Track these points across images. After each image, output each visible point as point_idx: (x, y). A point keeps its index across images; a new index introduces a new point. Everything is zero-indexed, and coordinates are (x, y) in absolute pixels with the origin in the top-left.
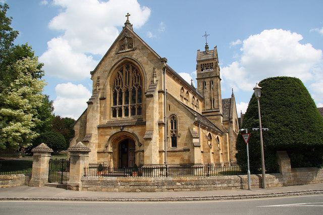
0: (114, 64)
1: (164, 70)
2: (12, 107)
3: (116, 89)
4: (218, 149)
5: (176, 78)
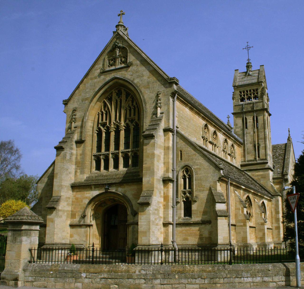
0: (97, 89)
1: (173, 97)
3: (102, 128)
4: (263, 221)
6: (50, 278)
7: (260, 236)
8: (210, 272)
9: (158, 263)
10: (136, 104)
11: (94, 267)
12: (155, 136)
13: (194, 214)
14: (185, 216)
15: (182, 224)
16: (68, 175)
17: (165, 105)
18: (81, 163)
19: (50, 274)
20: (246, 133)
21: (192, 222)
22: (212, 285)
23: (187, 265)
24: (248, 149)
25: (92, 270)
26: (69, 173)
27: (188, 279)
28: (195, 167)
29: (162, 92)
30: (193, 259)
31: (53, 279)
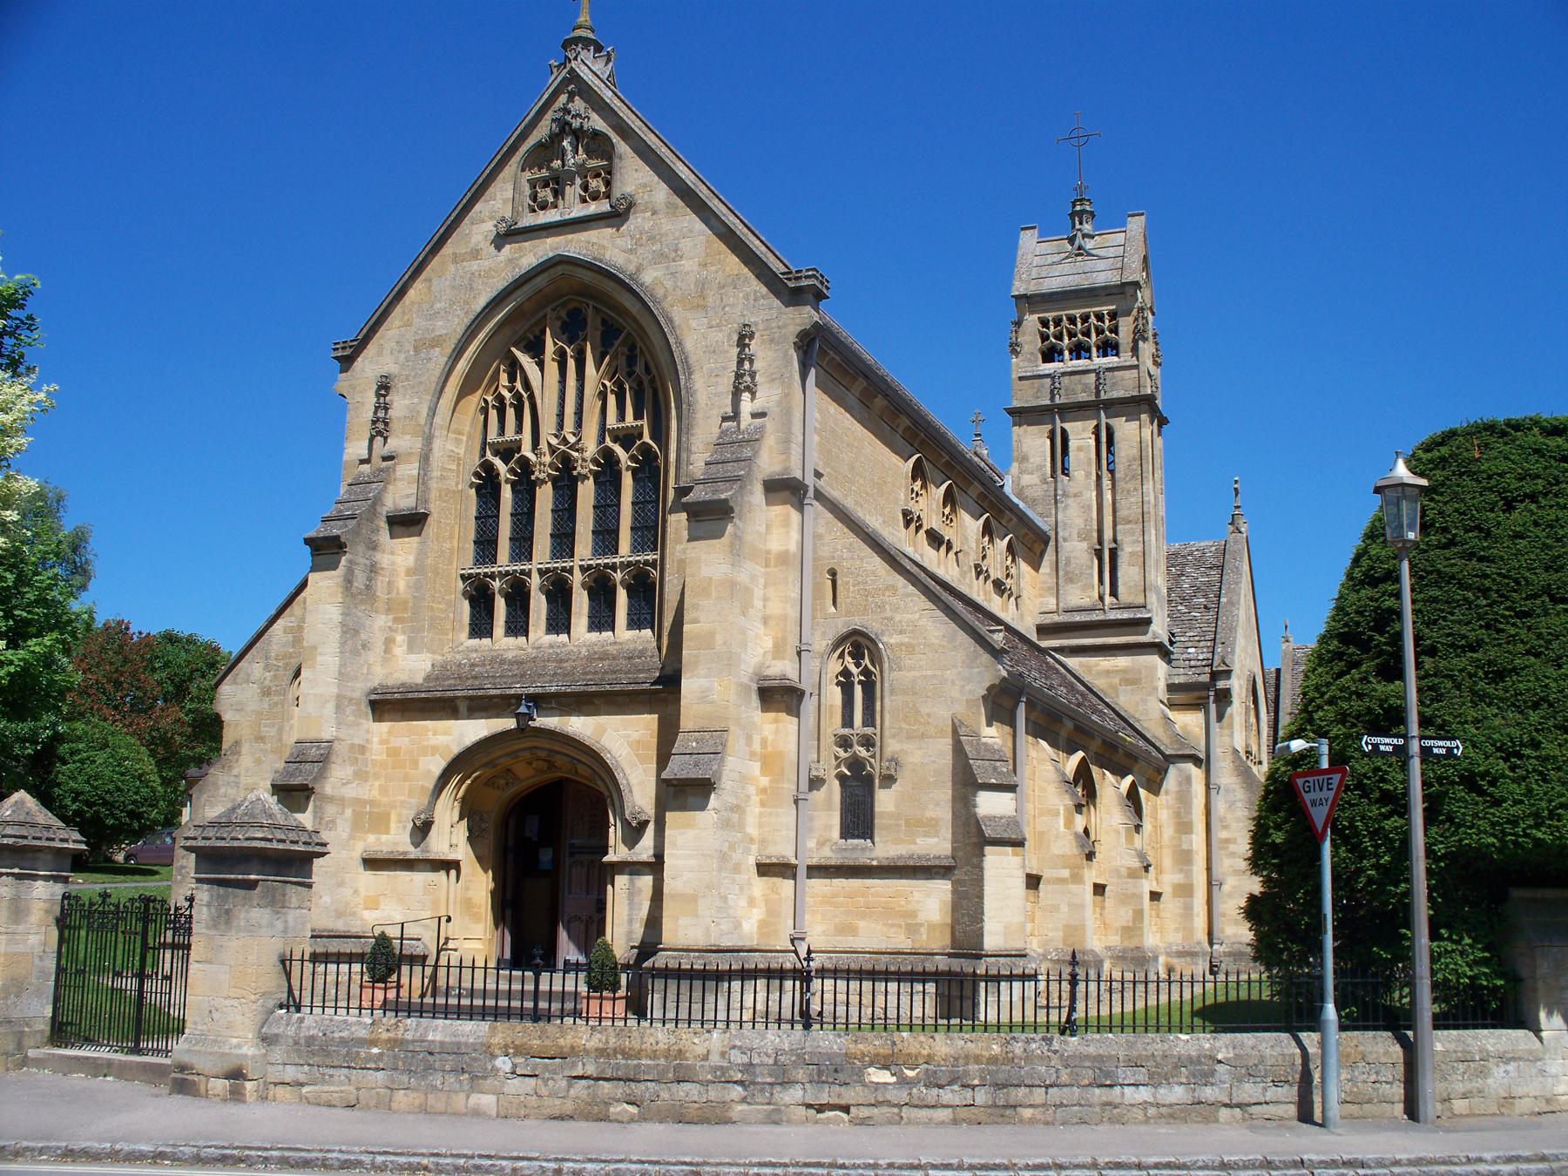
0: (482, 302)
5: (879, 402)
7: (1124, 924)
8: (993, 1060)
9: (1048, 1026)
10: (647, 370)
11: (543, 1031)
12: (736, 509)
14: (846, 833)
15: (832, 867)
16: (360, 655)
17: (773, 380)
19: (370, 1058)
20: (1065, 495)
22: (1002, 1111)
23: (905, 1034)
26: (364, 646)
28: (892, 641)
29: (761, 327)
30: (879, 1012)
31: (380, 1074)
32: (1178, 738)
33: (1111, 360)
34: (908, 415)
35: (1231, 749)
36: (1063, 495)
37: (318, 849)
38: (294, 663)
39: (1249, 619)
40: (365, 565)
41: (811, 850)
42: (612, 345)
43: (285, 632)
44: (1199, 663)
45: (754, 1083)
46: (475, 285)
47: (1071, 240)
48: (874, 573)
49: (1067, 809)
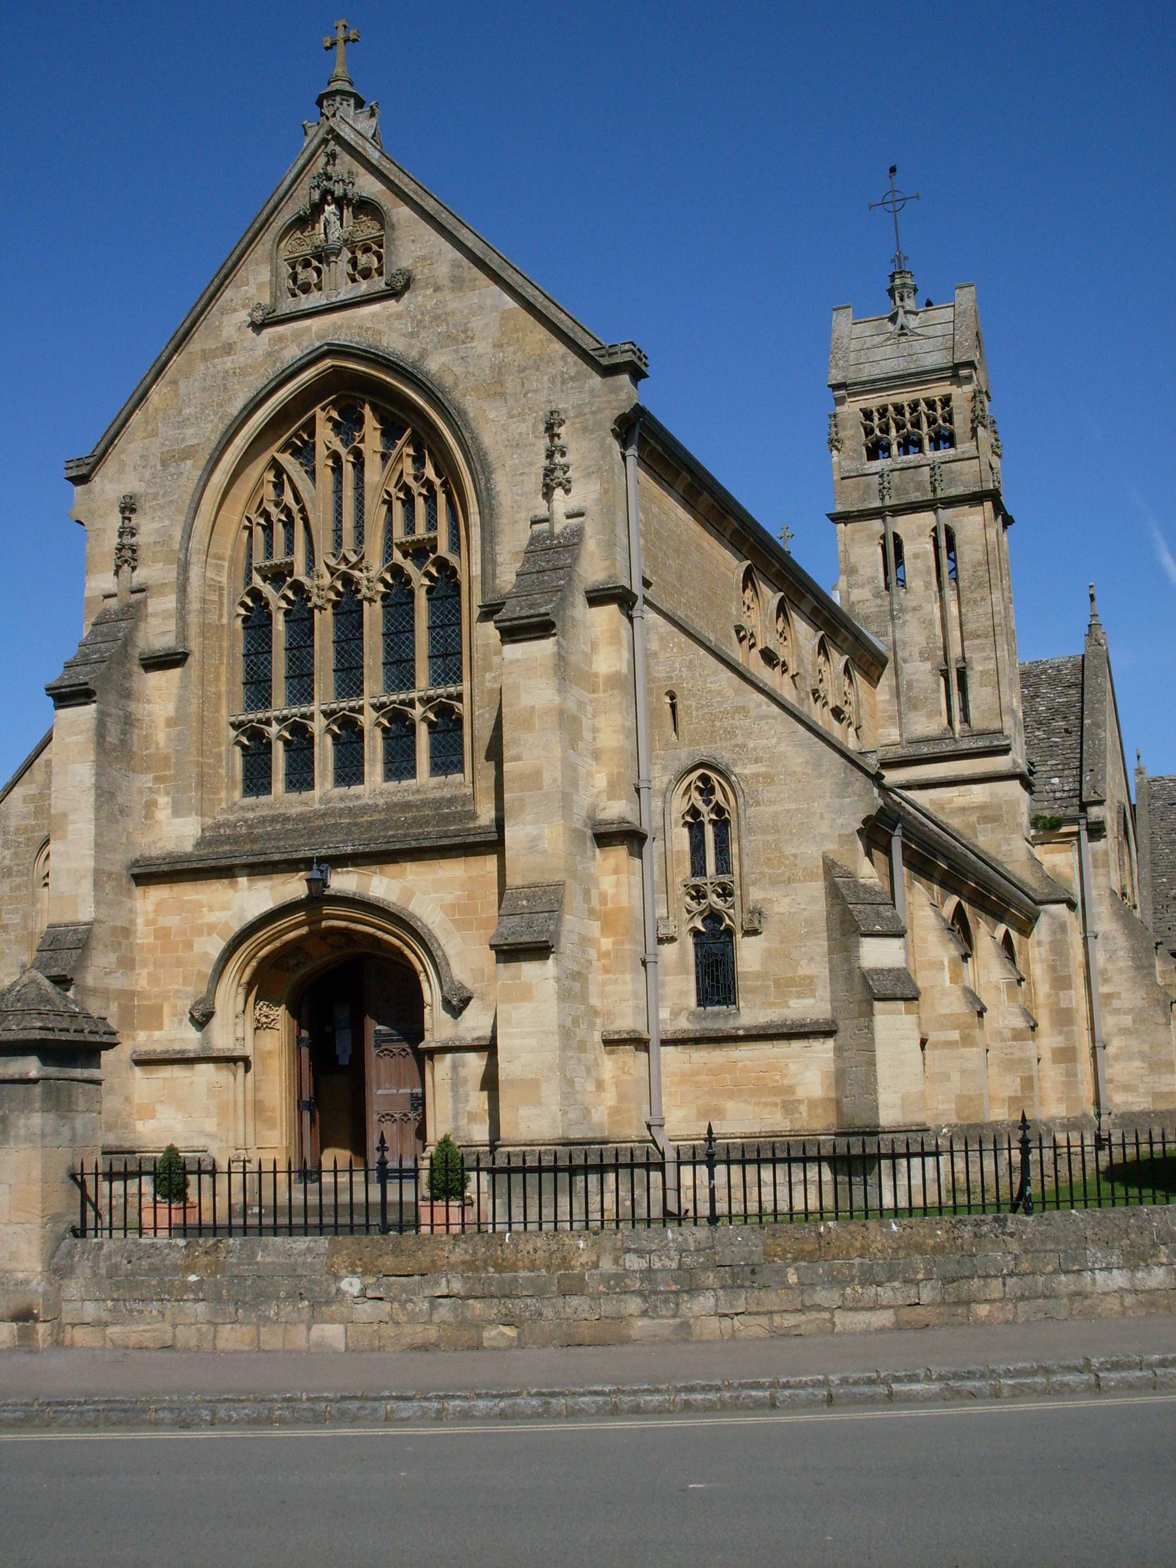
2: (183, 608)
5: (706, 499)
6: (189, 1304)
7: (1013, 1094)
11: (397, 1246)
12: (558, 624)
13: (753, 990)
14: (704, 998)
16: (117, 822)
17: (589, 475)
18: (173, 760)
19: (187, 1287)
21: (738, 1029)
24: (910, 687)
25: (389, 1262)
27: (844, 1289)
28: (746, 771)
32: (1049, 880)
33: (947, 453)
34: (736, 517)
35: (1108, 891)
36: (900, 610)
37: (105, 1039)
38: (40, 835)
39: (1114, 743)
40: (118, 716)
41: (664, 1021)
42: (394, 446)
43: (25, 801)
44: (1065, 795)
45: (656, 1293)
46: (229, 385)
47: (893, 319)
48: (719, 693)
49: (952, 960)
